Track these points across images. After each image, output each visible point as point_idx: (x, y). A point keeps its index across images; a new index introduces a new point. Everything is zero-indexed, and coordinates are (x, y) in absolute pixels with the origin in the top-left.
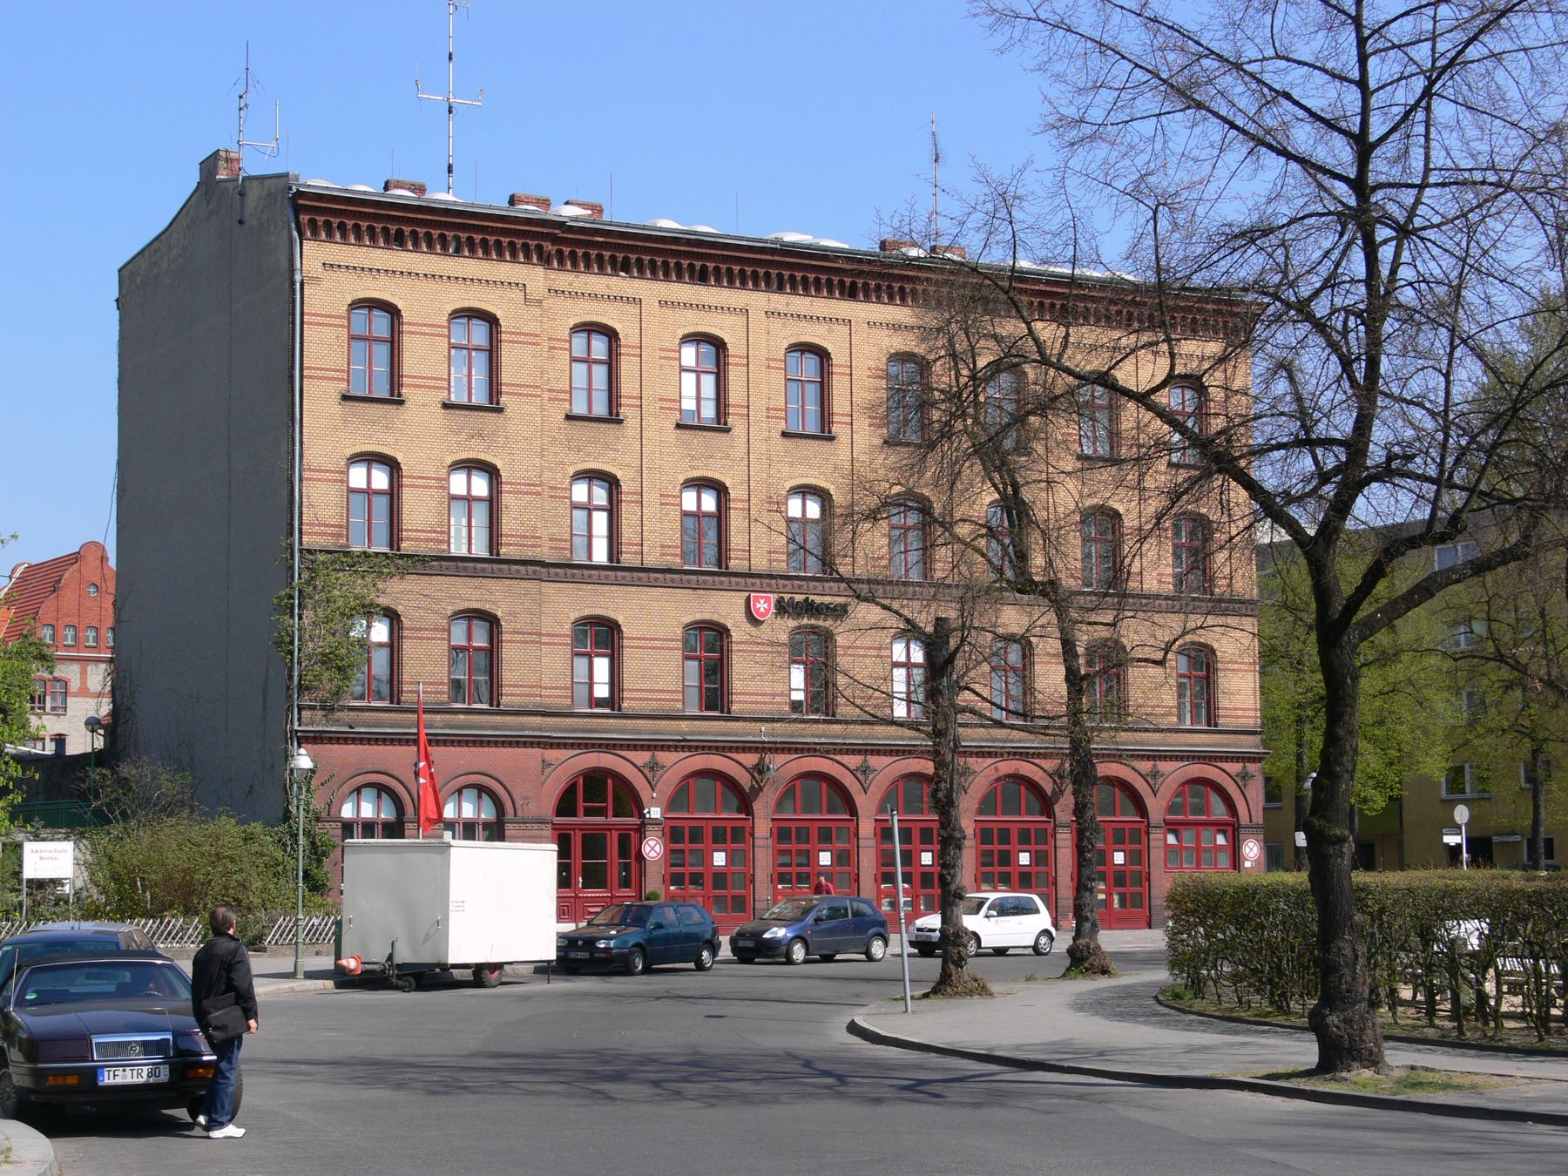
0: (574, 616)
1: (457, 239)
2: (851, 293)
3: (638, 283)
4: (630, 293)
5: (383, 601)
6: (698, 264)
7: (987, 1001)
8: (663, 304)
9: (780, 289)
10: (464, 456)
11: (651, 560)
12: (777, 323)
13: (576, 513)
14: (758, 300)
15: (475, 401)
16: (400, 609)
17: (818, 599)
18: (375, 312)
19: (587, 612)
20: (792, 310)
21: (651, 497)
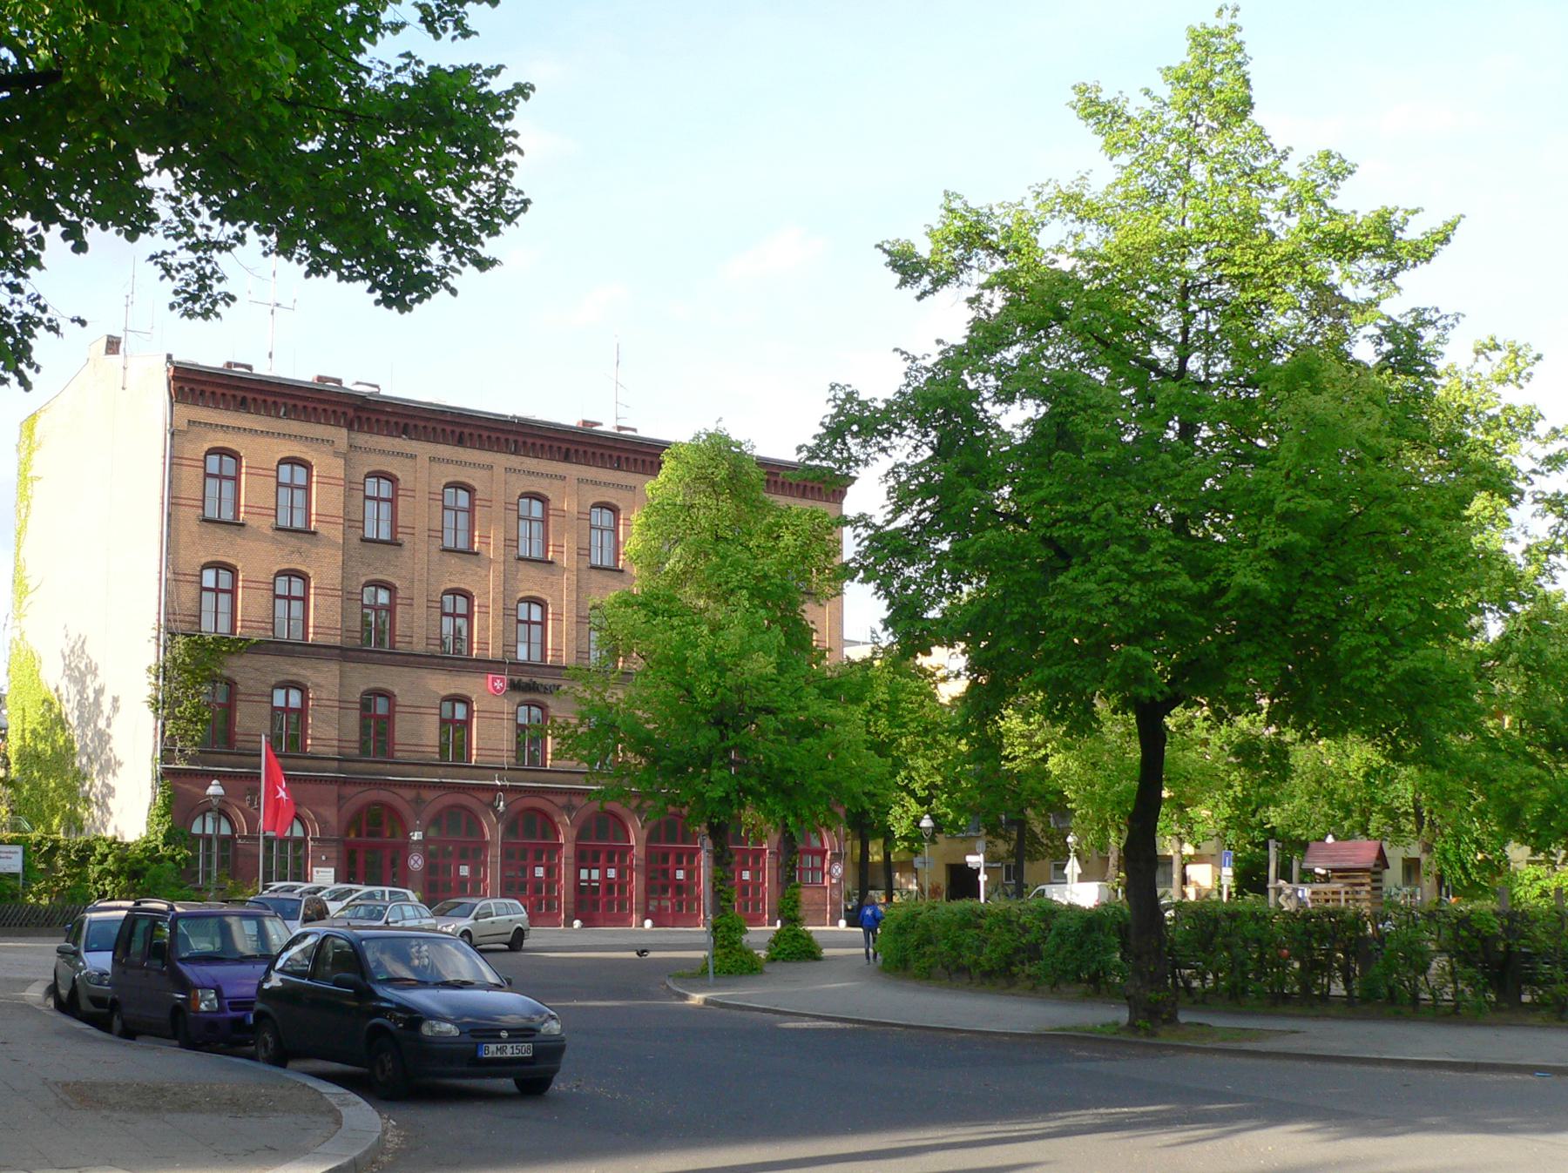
0: (363, 688)
1: (516, 442)
2: (566, 458)
3: (414, 443)
4: (409, 450)
5: (225, 673)
6: (458, 430)
7: (817, 964)
8: (432, 459)
9: (619, 468)
10: (286, 566)
11: (420, 648)
12: (513, 477)
13: (445, 619)
14: (501, 460)
15: (605, 564)
16: (237, 679)
17: (539, 681)
18: (296, 468)
19: (372, 685)
20: (524, 467)
21: (420, 601)
